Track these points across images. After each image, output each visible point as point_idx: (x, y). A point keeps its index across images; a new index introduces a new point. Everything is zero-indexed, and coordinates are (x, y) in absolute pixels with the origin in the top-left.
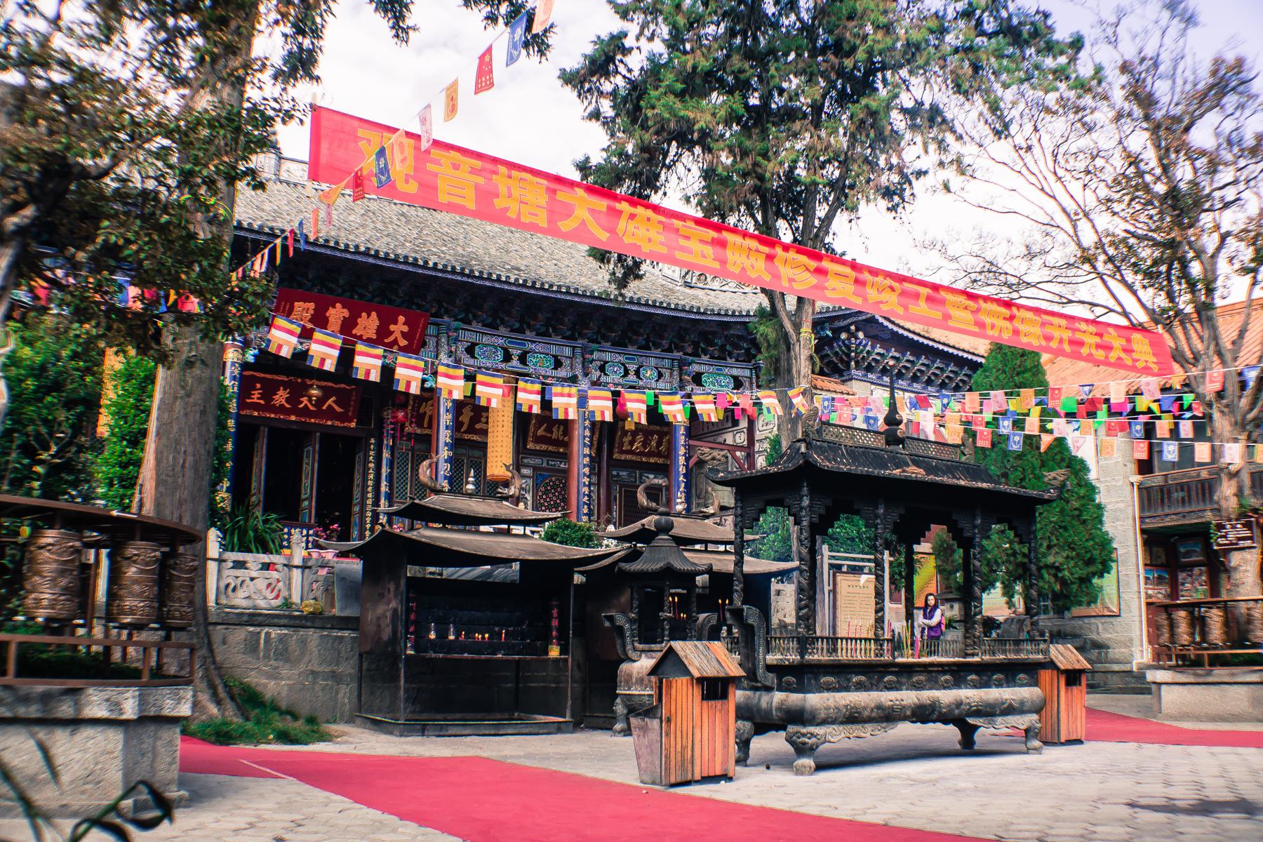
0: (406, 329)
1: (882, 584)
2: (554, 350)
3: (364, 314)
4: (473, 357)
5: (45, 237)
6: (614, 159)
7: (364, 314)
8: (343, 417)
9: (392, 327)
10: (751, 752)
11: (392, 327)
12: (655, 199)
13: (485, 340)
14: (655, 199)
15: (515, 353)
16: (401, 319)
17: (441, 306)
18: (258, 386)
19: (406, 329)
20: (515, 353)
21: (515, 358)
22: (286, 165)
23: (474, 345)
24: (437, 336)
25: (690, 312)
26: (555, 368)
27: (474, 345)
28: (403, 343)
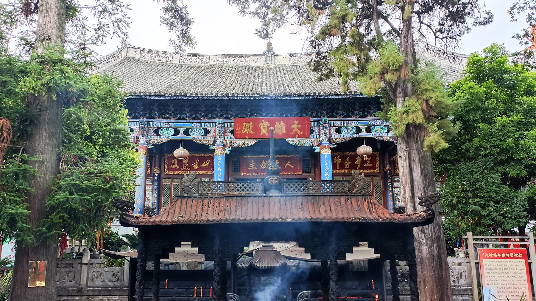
0: (299, 126)
1: (478, 239)
2: (204, 126)
3: (277, 123)
4: (340, 133)
5: (178, 116)
6: (247, 6)
7: (277, 123)
8: (295, 170)
9: (293, 127)
10: (261, 281)
11: (293, 127)
12: (378, 6)
13: (345, 124)
14: (378, 6)
15: (363, 128)
16: (296, 122)
17: (317, 112)
18: (253, 161)
19: (299, 126)
20: (181, 129)
21: (364, 130)
22: (278, 58)
23: (158, 129)
24: (319, 127)
25: (155, 95)
26: (388, 131)
27: (158, 129)
28: (300, 133)
